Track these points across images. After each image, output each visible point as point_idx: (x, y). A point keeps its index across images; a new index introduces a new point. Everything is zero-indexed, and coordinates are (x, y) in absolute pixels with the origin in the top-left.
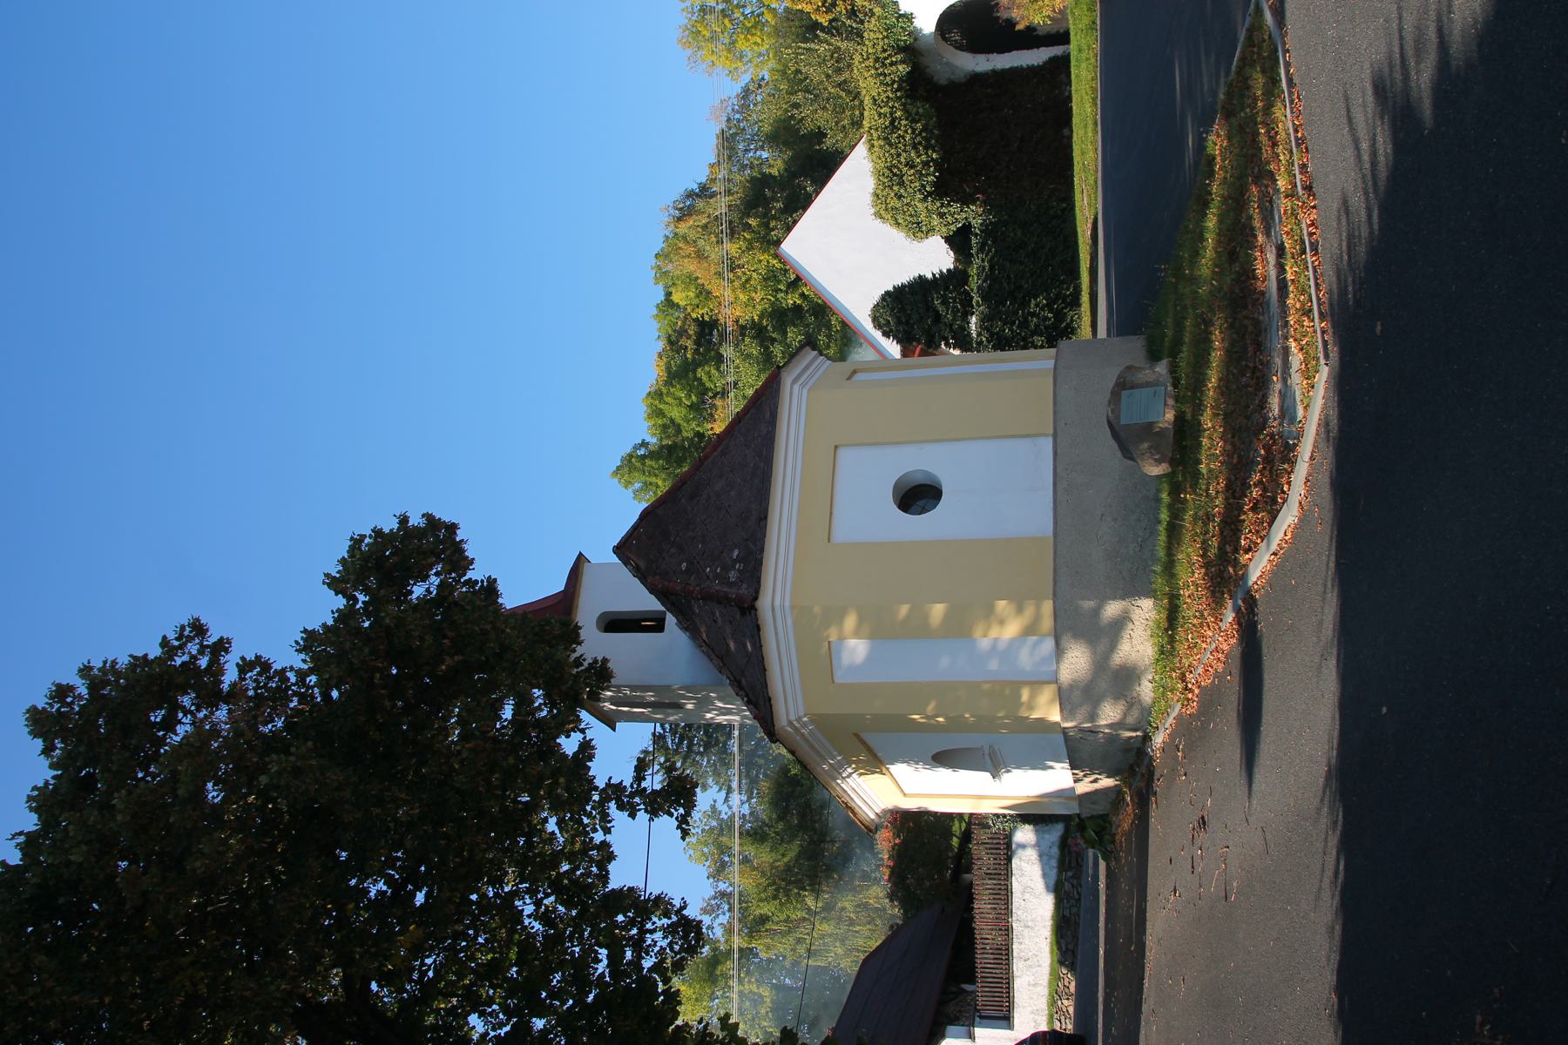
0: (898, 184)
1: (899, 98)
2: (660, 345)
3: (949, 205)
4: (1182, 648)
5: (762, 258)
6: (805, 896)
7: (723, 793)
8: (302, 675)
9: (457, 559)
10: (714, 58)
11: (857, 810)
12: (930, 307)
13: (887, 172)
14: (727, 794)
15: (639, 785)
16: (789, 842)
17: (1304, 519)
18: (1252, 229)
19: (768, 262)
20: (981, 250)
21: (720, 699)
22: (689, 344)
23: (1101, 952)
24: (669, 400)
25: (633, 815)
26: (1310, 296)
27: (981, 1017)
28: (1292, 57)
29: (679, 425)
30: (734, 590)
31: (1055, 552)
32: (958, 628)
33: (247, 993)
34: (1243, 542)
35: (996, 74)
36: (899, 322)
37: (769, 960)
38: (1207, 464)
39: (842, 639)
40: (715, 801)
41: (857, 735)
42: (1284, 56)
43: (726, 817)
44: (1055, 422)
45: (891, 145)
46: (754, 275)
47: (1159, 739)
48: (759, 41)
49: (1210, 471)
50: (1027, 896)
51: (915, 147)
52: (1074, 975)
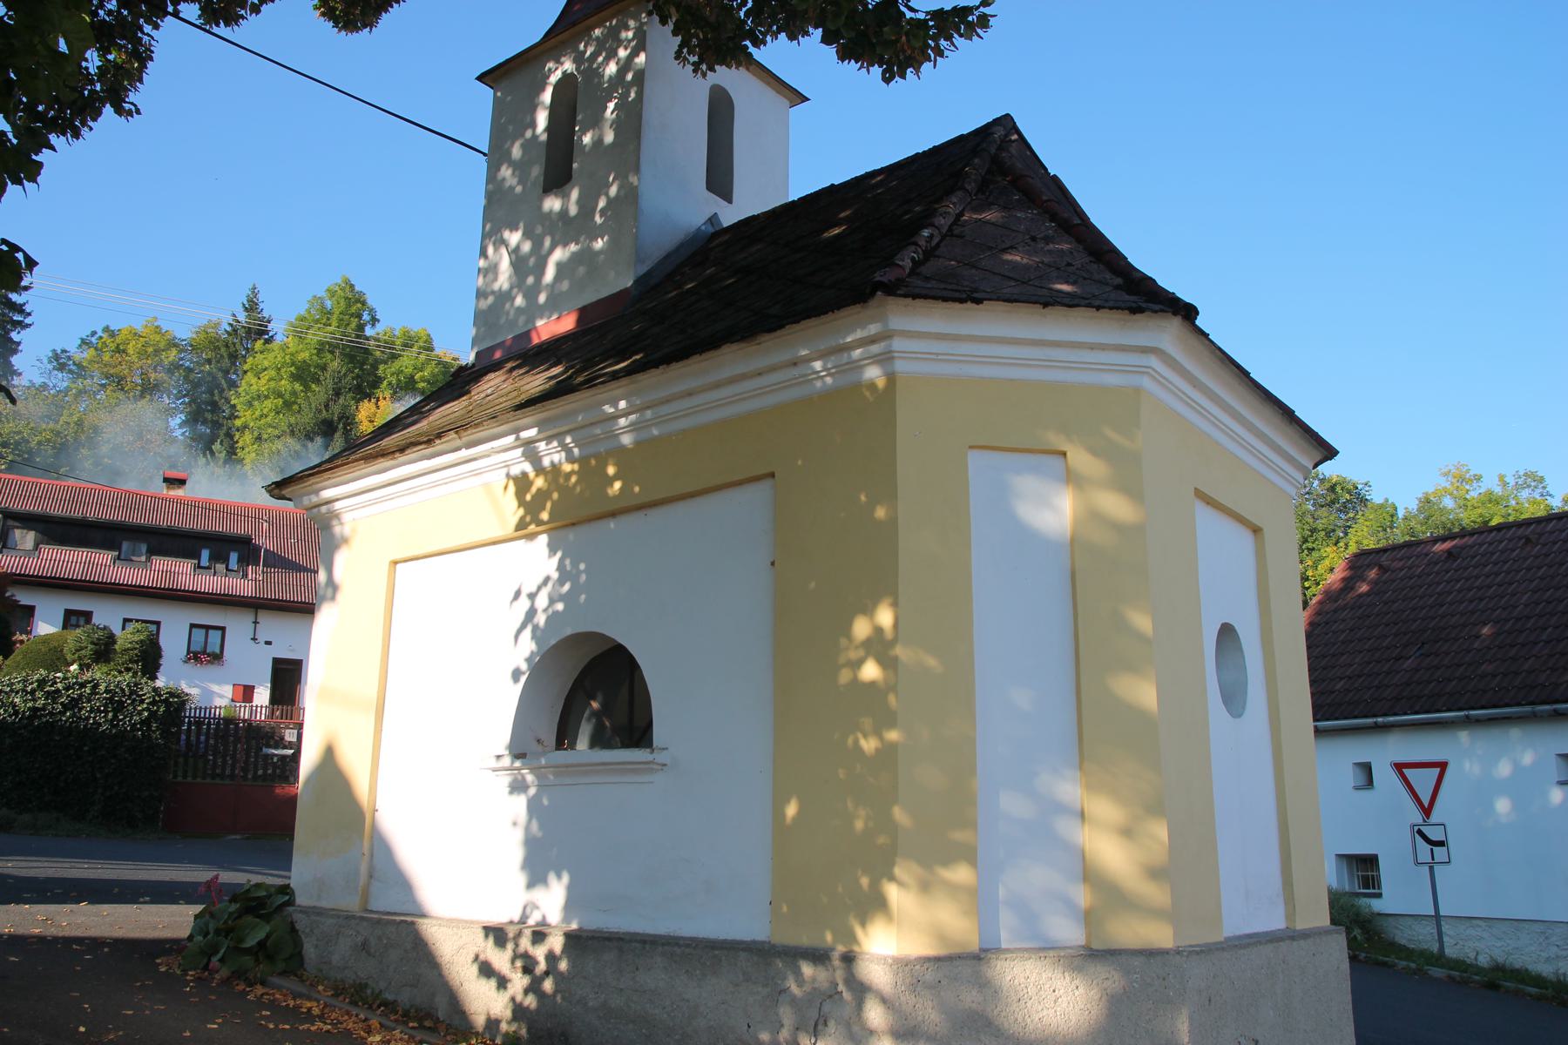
39: (1071, 478)
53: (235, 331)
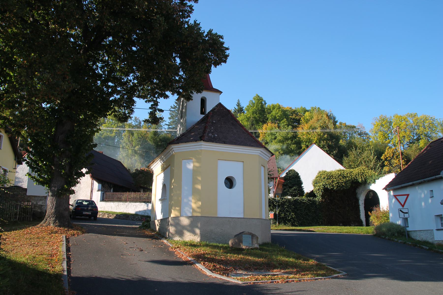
0: (328, 178)
1: (352, 179)
2: (294, 108)
3: (322, 192)
4: (185, 248)
5: (316, 138)
6: (139, 146)
7: (168, 124)
8: (187, 22)
9: (217, 64)
10: (376, 125)
11: (153, 164)
12: (294, 185)
13: (331, 175)
14: (168, 125)
15: (157, 110)
16: (154, 142)
17: (207, 276)
18: (285, 269)
19: (314, 140)
20: (309, 200)
21: (183, 129)
22: (294, 117)
23: (117, 225)
24: (277, 111)
25: (150, 108)
26: (260, 281)
27: (103, 193)
28: (323, 280)
29: (270, 113)
30: (206, 135)
31: (250, 218)
32: (195, 192)
33: (104, 14)
34: (206, 263)
35: (358, 206)
36: (290, 177)
37: (122, 135)
38: (229, 256)
39: (193, 162)
40: (166, 121)
41: (170, 165)
42: (323, 278)
43: (161, 124)
44: (247, 218)
45: (339, 176)
46: (311, 136)
47: (165, 241)
48: (381, 138)
49: (228, 256)
50: (135, 206)
51: (338, 183)
52: (114, 218)
53: (235, 111)
